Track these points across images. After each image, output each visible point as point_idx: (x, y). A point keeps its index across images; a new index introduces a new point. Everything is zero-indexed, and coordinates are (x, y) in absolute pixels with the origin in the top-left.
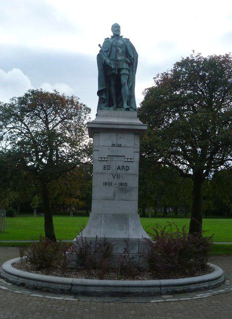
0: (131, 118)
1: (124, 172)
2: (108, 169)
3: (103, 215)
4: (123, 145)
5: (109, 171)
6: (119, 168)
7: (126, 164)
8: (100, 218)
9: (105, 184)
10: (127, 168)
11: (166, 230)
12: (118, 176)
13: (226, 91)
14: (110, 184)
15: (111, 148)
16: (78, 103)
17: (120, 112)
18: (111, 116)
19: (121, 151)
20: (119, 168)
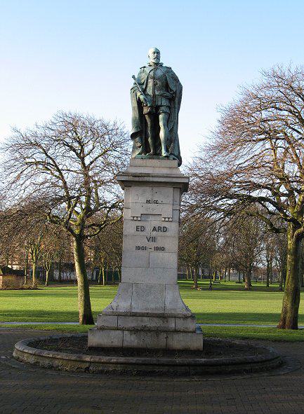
1: (160, 233)
5: (142, 233)
6: (154, 229)
9: (138, 248)
10: (165, 230)
12: (154, 239)
14: (144, 248)
17: (155, 162)
20: (154, 229)
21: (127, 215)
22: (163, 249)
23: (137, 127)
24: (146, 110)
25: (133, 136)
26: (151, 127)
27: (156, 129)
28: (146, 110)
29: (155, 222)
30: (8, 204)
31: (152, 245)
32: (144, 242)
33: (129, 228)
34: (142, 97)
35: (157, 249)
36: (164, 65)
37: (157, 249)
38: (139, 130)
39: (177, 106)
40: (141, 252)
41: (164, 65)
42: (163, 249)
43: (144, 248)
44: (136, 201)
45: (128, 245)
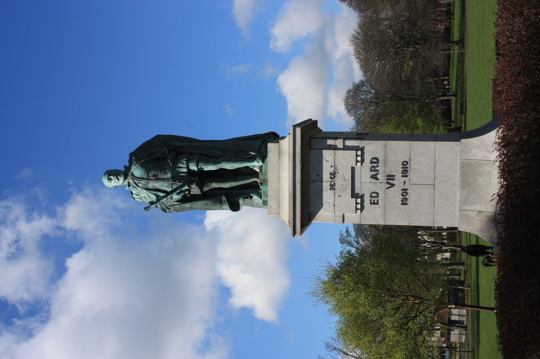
0: (280, 154)
1: (380, 168)
2: (378, 197)
3: (464, 208)
4: (332, 170)
5: (381, 196)
6: (374, 177)
7: (367, 164)
8: (469, 213)
9: (404, 202)
10: (375, 161)
11: (334, 313)
12: (390, 177)
13: (377, 272)
14: (405, 192)
15: (338, 193)
16: (498, 278)
17: (271, 176)
18: (279, 190)
19: (344, 175)
20: (374, 177)
21: (354, 218)
22: (405, 165)
23: (221, 202)
24: (195, 190)
25: (235, 207)
26: (220, 182)
27: (222, 175)
28: (195, 190)
29: (364, 174)
30: (502, 357)
31: (399, 181)
32: (396, 193)
33: (374, 216)
34: (176, 197)
35: (405, 172)
36: (127, 164)
37: (405, 172)
38: (224, 198)
39: (187, 144)
40: (411, 197)
41: (127, 164)
42: (405, 165)
43: (405, 192)
44: (337, 213)
45: (398, 218)
